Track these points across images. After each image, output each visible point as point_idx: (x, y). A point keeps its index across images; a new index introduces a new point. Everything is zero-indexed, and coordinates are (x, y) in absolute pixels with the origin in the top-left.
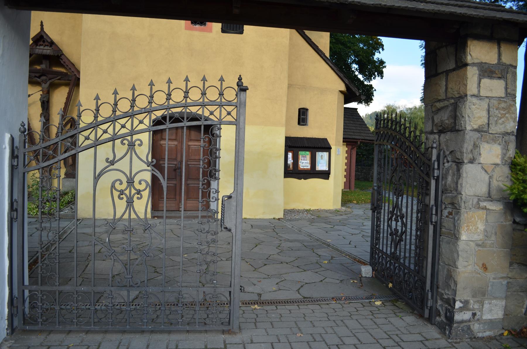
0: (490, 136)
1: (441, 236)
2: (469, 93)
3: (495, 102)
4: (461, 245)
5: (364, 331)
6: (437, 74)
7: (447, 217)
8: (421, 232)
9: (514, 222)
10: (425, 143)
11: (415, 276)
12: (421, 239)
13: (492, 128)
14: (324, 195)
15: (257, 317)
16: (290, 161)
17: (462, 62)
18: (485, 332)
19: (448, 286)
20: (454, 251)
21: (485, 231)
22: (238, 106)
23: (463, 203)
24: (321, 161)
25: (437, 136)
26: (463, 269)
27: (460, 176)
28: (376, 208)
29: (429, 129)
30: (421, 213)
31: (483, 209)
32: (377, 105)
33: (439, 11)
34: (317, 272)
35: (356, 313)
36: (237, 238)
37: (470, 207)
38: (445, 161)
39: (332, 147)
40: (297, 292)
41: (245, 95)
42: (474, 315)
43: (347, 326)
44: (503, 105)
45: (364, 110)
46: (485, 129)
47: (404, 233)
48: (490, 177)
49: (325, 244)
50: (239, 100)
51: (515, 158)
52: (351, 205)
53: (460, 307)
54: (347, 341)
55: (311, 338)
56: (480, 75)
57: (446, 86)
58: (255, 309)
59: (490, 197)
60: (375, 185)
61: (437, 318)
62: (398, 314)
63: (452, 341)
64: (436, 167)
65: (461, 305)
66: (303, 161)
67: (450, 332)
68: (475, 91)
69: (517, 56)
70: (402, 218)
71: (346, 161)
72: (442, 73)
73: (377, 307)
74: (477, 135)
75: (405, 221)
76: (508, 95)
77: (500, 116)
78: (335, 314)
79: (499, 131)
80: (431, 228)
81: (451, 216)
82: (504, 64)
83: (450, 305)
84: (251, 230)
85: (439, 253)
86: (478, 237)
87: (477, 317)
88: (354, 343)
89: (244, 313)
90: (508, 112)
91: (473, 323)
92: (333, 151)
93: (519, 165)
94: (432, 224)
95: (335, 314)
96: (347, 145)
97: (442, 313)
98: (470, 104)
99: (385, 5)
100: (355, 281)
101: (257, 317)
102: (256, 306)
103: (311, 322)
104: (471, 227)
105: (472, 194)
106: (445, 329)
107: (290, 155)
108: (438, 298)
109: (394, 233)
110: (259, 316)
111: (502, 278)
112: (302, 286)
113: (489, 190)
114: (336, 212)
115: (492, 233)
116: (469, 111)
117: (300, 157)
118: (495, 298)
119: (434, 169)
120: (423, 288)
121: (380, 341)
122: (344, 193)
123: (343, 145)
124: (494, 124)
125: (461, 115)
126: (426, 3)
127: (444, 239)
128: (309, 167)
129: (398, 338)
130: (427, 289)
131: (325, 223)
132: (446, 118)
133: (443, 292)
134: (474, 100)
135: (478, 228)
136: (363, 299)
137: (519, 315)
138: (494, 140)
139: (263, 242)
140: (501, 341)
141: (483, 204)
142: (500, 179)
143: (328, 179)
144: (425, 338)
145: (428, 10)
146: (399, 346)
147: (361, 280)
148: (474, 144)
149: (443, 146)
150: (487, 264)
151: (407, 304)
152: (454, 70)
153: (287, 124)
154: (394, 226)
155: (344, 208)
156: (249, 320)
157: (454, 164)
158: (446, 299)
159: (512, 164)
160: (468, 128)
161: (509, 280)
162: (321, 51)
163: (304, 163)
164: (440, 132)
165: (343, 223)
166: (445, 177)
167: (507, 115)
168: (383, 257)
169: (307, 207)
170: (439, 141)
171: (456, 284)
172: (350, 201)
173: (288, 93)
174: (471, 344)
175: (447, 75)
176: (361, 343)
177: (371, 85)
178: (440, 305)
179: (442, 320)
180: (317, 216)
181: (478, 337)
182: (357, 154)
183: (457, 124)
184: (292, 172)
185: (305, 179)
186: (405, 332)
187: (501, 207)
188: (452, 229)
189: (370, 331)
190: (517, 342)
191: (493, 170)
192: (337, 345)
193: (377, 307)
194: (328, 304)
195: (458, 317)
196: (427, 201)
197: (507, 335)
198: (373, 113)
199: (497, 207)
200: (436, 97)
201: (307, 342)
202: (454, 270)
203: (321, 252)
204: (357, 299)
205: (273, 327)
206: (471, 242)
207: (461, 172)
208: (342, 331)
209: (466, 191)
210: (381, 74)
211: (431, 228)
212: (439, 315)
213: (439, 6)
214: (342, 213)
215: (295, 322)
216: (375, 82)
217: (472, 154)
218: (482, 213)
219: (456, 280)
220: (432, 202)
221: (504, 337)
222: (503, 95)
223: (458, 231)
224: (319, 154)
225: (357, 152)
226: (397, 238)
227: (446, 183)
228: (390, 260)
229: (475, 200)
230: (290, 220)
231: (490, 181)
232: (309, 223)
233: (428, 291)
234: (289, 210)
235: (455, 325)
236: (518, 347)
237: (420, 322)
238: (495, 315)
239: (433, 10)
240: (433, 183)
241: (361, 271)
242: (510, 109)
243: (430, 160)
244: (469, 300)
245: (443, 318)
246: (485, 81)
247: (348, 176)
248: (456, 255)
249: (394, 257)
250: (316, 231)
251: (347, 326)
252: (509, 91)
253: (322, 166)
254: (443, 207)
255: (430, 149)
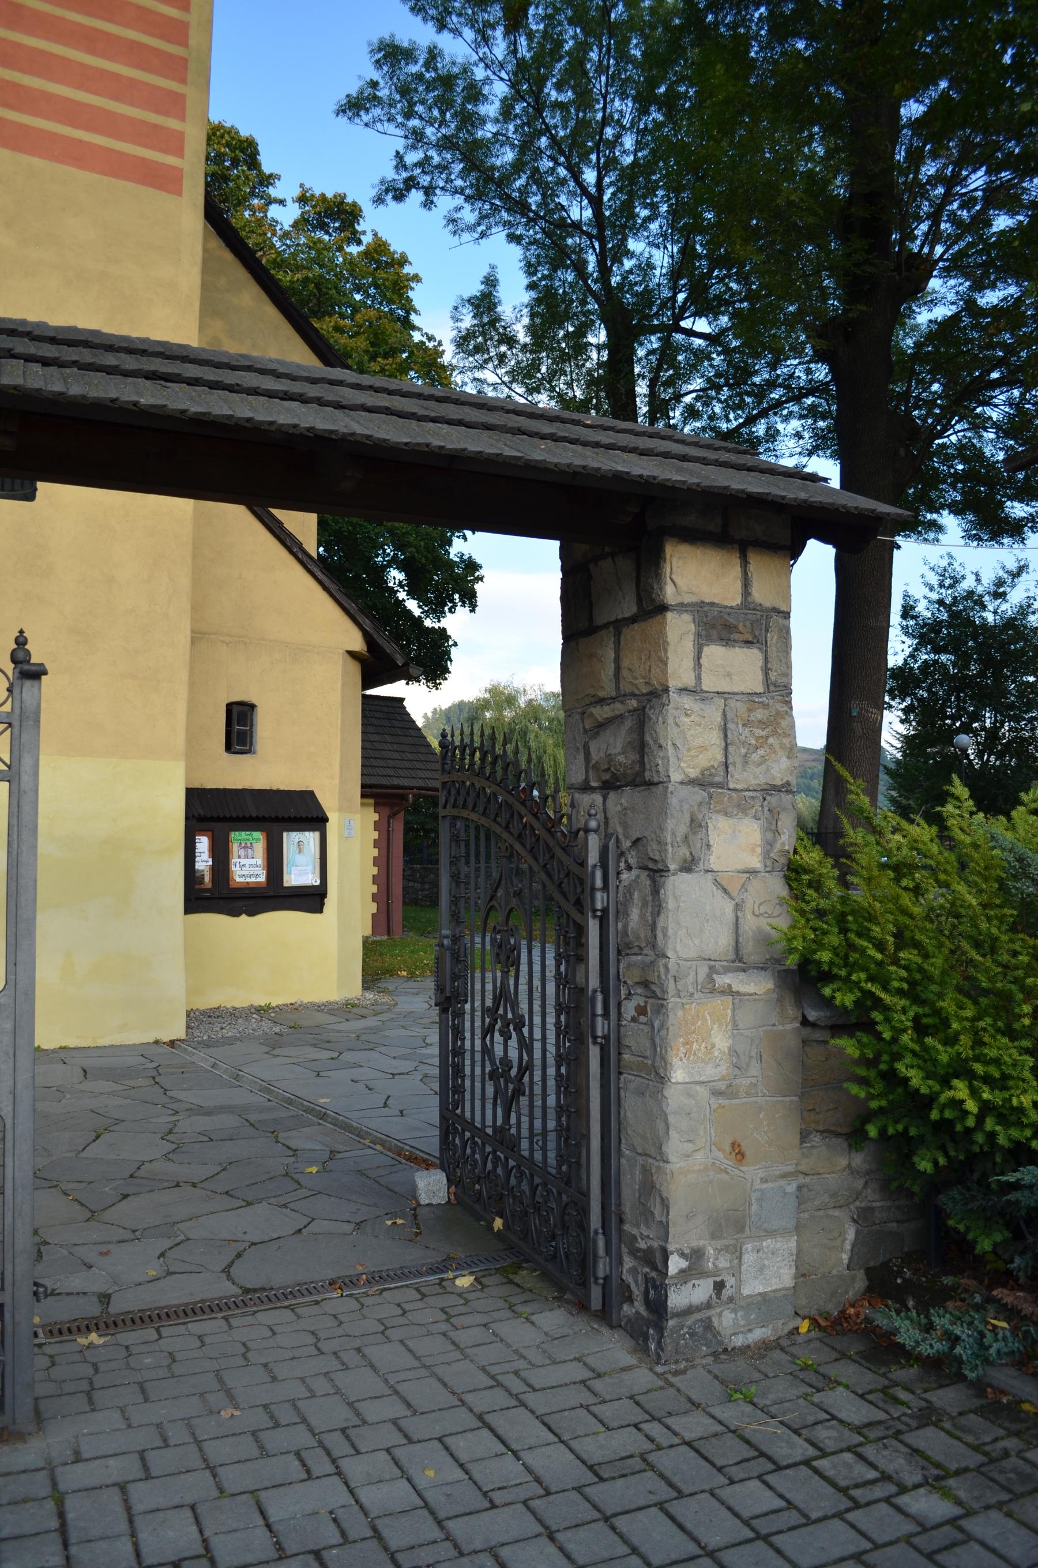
0: (730, 797)
1: (620, 1073)
2: (672, 683)
3: (739, 707)
4: (674, 1098)
5: (423, 1372)
6: (592, 630)
7: (634, 1019)
8: (568, 1065)
9: (805, 1022)
10: (570, 818)
11: (560, 1194)
12: (571, 1086)
13: (737, 776)
14: (310, 958)
15: (97, 1371)
16: (204, 861)
17: (653, 600)
18: (750, 1330)
19: (647, 1215)
20: (658, 1116)
21: (733, 1051)
22: (16, 724)
23: (672, 981)
24: (300, 859)
25: (598, 798)
26: (683, 1164)
27: (660, 906)
28: (449, 1002)
29: (577, 776)
30: (568, 1013)
31: (723, 993)
32: (465, 682)
33: (584, 467)
34: (285, 1206)
35: (402, 1321)
36: (18, 1132)
37: (691, 990)
38: (622, 865)
39: (329, 815)
40: (224, 1275)
41: (35, 690)
42: (719, 1286)
43: (372, 1366)
44: (760, 714)
45: (420, 701)
46: (717, 779)
47: (525, 1068)
48: (738, 907)
49: (310, 1111)
50: (17, 705)
51: (795, 852)
52: (390, 984)
53: (682, 1271)
54: (373, 1411)
55: (266, 1417)
56: (699, 635)
57: (617, 660)
58: (91, 1346)
59: (739, 962)
60: (446, 932)
61: (625, 1307)
62: (519, 1308)
63: (666, 1368)
64: (599, 883)
65: (684, 1264)
66: (243, 861)
67: (659, 1345)
68: (687, 678)
69: (789, 587)
70: (519, 1028)
71: (375, 852)
72: (606, 626)
73: (460, 1295)
74: (700, 794)
75: (526, 1034)
76: (772, 688)
77: (753, 742)
78: (340, 1331)
79: (753, 782)
80: (594, 1052)
81: (643, 1019)
82: (758, 608)
83: (654, 1268)
84: (81, 1087)
85: (620, 1123)
86: (715, 1071)
87: (726, 1293)
88: (392, 1416)
89: (53, 1364)
90: (774, 733)
91: (718, 1310)
92: (332, 828)
93: (807, 871)
94: (595, 1043)
95: (340, 1331)
96: (377, 807)
97: (637, 1292)
98: (676, 713)
99: (441, 448)
100: (399, 1221)
101: (97, 1371)
102: (94, 1337)
103: (265, 1365)
104: (695, 1046)
105: (692, 954)
106: (646, 1337)
107: (203, 844)
108: (624, 1250)
109: (499, 1073)
110: (102, 1367)
111: (784, 1176)
112: (239, 1255)
113: (737, 942)
114: (347, 1009)
115: (751, 1057)
116: (676, 730)
117: (235, 848)
118: (771, 1233)
119: (593, 889)
120: (583, 1226)
121: (469, 1398)
122: (369, 947)
123: (362, 804)
124: (739, 766)
125: (655, 741)
126: (555, 441)
127: (630, 1081)
128: (262, 878)
129: (518, 1381)
130: (593, 1228)
131: (314, 1045)
132: (618, 750)
133: (635, 1231)
134: (687, 702)
135: (713, 1046)
136: (421, 1274)
137: (834, 1272)
138: (743, 808)
139: (118, 1121)
140: (794, 1350)
141: (723, 980)
142: (763, 909)
143: (321, 911)
144: (593, 1370)
145: (556, 465)
146: (523, 1404)
147: (415, 1216)
148: (692, 820)
149: (616, 826)
150: (743, 1144)
151: (545, 1275)
152: (634, 620)
153: (192, 752)
154: (499, 1050)
155: (370, 995)
156: (69, 1388)
157: (644, 874)
158: (644, 1251)
159: (789, 869)
160: (676, 777)
161: (802, 1180)
162: (290, 535)
163: (248, 866)
164: (608, 786)
165: (366, 1043)
166: (622, 911)
167: (771, 740)
168: (475, 1143)
169: (261, 1000)
170: (605, 812)
171: (666, 1206)
172: (390, 972)
173: (192, 656)
174: (716, 1371)
175: (618, 634)
176: (415, 1413)
177: (444, 630)
178: (630, 1271)
179: (637, 1313)
180: (289, 1027)
181: (733, 1349)
182: (408, 830)
183: (647, 766)
184: (210, 894)
185: (251, 914)
186: (538, 1359)
187: (770, 985)
188: (648, 1053)
189: (440, 1370)
190: (834, 1349)
191: (743, 885)
192: (343, 1431)
193: (460, 1295)
194: (317, 1303)
195: (677, 1299)
196: (580, 979)
197: (809, 1331)
198: (454, 705)
199: (758, 985)
200: (592, 691)
201: (254, 1433)
202: (658, 1168)
203: (299, 1139)
204: (404, 1276)
205: (146, 1400)
206: (698, 1088)
207: (662, 896)
208: (359, 1382)
209: (678, 948)
210: (470, 599)
211: (594, 1052)
212: (630, 1299)
213: (588, 451)
214: (363, 1012)
215: (217, 1374)
216: (456, 622)
217: (689, 846)
218: (722, 1005)
219: (665, 1195)
220: (594, 982)
221: (800, 1339)
222: (760, 689)
223: (663, 1059)
224: (291, 840)
225: (406, 823)
226: (510, 1083)
227: (625, 927)
228: (495, 1152)
229: (703, 971)
230: (207, 1045)
231: (737, 918)
232: (267, 1049)
233: (596, 1232)
234: (203, 1013)
235: (671, 1323)
236: (836, 1360)
237: (581, 1324)
238: (774, 1281)
239: (569, 465)
240: (593, 927)
241: (414, 1188)
242: (778, 724)
243: (583, 864)
244: (704, 1246)
245: (639, 1306)
246: (714, 652)
247: (383, 898)
248: (661, 1126)
249: (504, 1139)
250: (287, 1072)
251: (372, 1366)
252: (773, 676)
253: (300, 872)
254: (623, 993)
255: (581, 833)
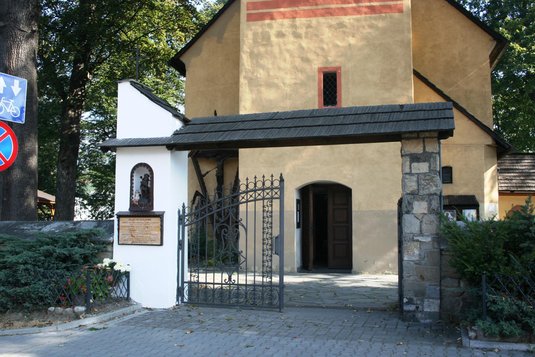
42: (417, 308)
138: (423, 199)
246: (415, 165)
